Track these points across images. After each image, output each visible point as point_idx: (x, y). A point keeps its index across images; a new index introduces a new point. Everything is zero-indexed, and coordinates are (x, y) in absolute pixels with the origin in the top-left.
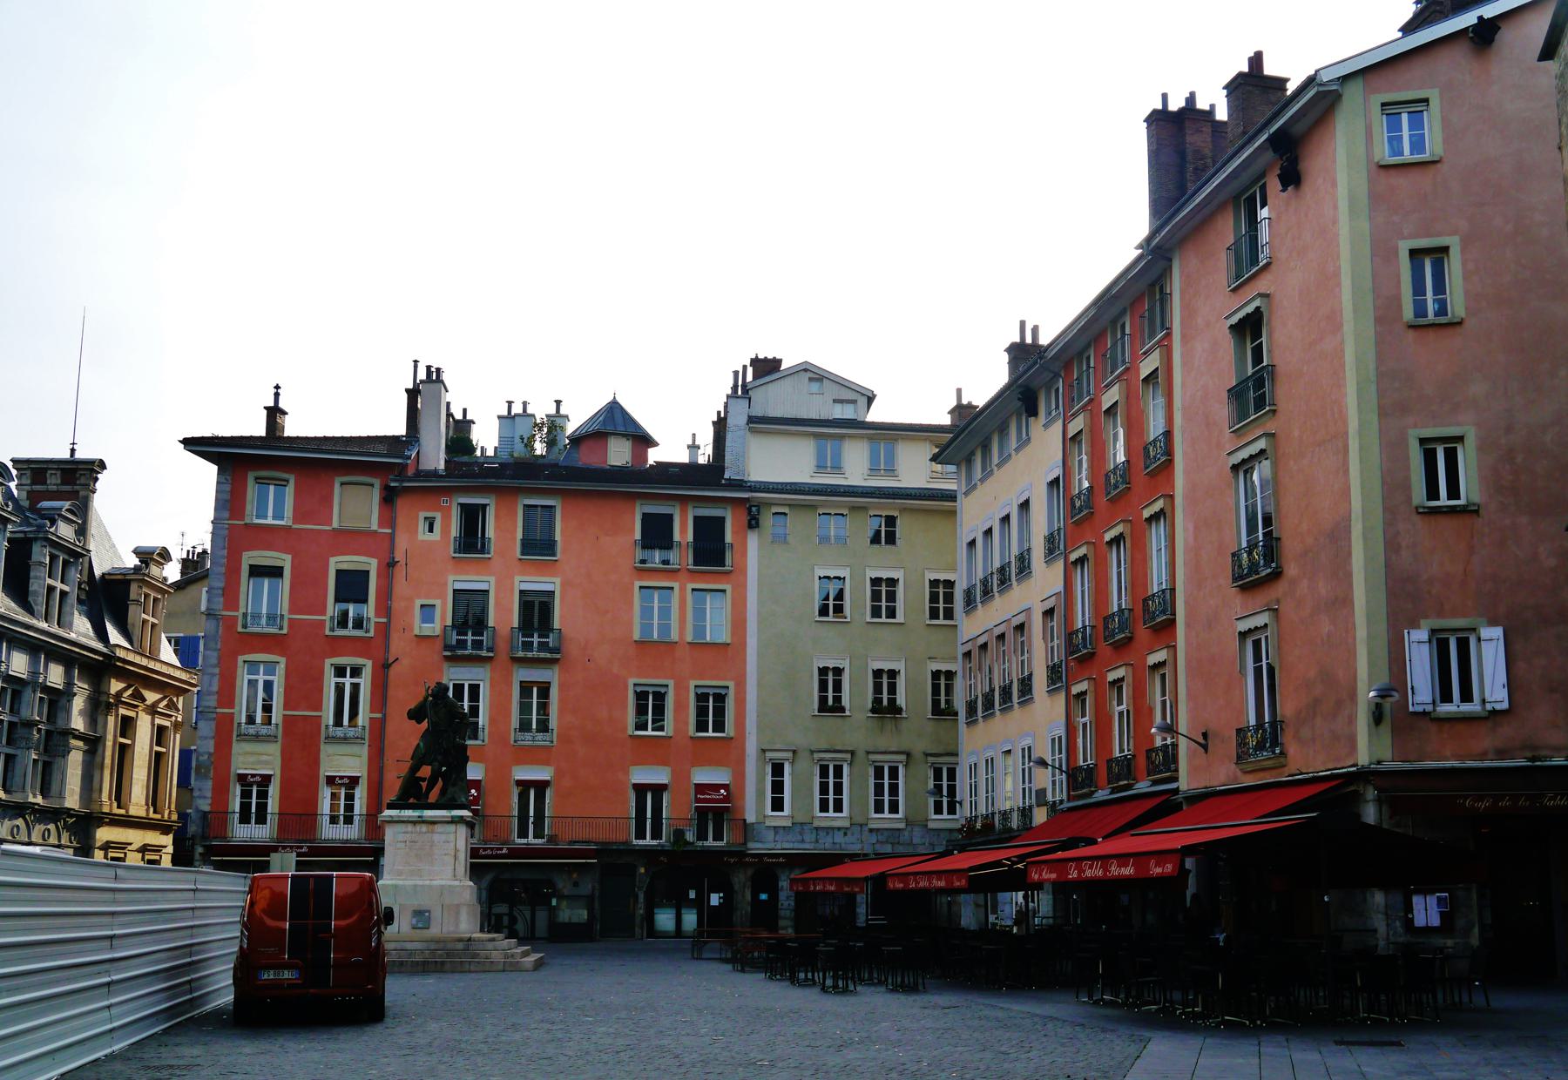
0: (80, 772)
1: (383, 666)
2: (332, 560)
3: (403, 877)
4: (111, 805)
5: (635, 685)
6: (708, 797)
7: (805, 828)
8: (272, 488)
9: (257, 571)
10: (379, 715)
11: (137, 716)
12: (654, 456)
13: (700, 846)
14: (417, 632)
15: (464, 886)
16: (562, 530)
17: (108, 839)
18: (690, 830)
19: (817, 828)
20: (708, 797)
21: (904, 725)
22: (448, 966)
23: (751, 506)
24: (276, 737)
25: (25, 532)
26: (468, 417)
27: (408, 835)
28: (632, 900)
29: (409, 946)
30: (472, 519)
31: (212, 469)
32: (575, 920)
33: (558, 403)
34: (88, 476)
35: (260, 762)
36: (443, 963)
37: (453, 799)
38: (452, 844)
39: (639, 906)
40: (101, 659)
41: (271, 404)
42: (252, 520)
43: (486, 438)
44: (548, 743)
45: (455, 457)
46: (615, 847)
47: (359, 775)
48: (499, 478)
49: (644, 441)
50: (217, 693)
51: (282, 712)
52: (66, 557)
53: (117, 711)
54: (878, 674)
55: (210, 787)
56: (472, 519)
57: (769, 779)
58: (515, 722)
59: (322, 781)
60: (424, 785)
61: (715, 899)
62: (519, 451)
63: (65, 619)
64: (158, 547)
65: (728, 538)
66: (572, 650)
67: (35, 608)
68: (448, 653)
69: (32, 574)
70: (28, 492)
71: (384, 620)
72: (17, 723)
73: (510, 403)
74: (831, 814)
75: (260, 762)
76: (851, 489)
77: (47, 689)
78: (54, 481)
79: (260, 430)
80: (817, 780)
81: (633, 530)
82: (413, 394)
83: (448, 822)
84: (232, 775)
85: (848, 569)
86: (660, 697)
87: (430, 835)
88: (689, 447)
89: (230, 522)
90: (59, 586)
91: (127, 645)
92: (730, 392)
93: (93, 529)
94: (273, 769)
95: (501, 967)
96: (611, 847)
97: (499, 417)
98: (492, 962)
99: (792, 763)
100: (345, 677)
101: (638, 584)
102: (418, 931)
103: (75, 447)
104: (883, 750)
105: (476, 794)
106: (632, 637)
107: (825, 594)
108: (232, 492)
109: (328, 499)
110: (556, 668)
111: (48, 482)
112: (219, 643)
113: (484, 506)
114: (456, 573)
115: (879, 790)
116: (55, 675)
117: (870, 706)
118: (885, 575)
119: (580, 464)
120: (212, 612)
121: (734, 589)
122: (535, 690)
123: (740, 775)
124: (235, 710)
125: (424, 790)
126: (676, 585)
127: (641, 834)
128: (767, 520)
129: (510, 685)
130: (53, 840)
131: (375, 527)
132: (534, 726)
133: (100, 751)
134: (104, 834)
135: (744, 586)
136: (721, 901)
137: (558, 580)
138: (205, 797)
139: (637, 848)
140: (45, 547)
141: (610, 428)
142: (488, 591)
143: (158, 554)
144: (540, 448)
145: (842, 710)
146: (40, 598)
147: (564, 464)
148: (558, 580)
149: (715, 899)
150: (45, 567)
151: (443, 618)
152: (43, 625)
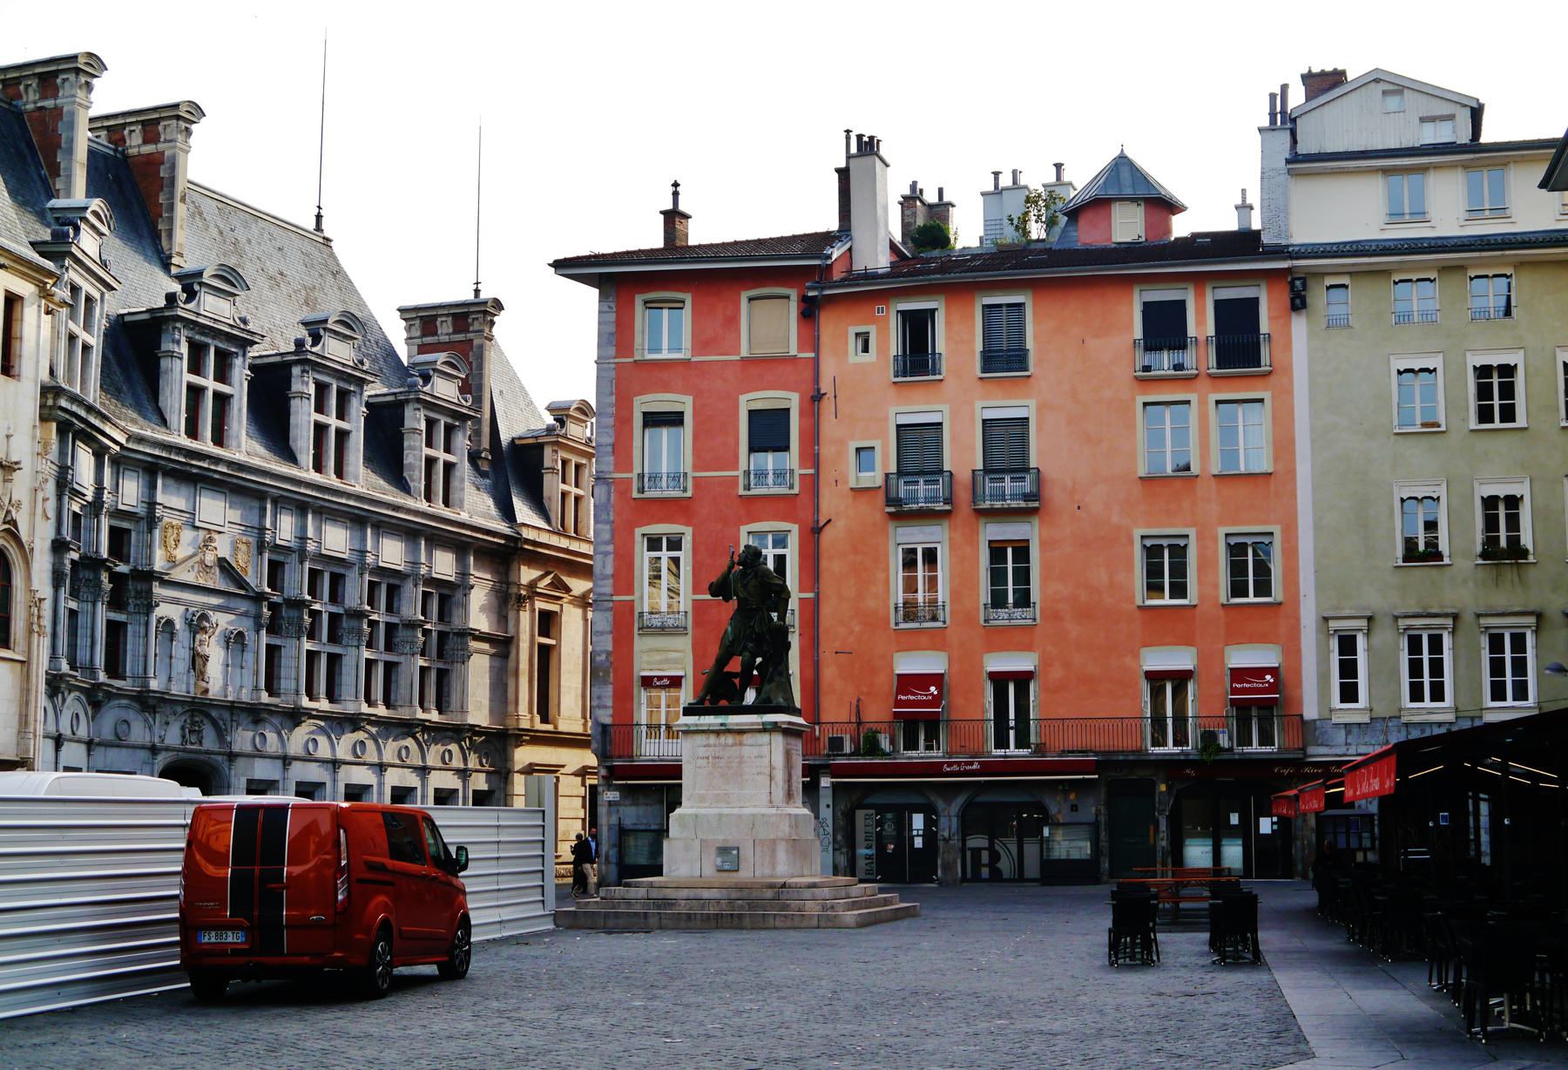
0: (487, 681)
1: (812, 529)
2: (743, 399)
3: (708, 804)
4: (532, 720)
5: (1143, 537)
6: (1247, 685)
7: (1390, 724)
9: (653, 420)
10: (811, 595)
11: (562, 610)
12: (1181, 227)
13: (1239, 754)
14: (853, 484)
15: (781, 815)
16: (1035, 337)
17: (532, 761)
18: (1223, 732)
19: (1406, 725)
20: (1247, 685)
21: (1532, 573)
22: (747, 922)
23: (1294, 279)
24: (685, 628)
25: (395, 394)
26: (946, 199)
27: (711, 749)
28: (1152, 827)
29: (706, 894)
30: (917, 329)
31: (592, 293)
32: (1075, 855)
33: (1058, 166)
34: (481, 320)
35: (667, 661)
36: (740, 916)
37: (769, 700)
38: (767, 760)
39: (1161, 835)
40: (503, 542)
41: (670, 207)
42: (643, 355)
43: (967, 232)
44: (1029, 622)
45: (922, 252)
46: (1121, 758)
47: (680, 673)
48: (945, 273)
49: (1164, 206)
50: (613, 576)
52: (449, 420)
53: (532, 605)
54: (1490, 503)
55: (611, 694)
56: (917, 329)
57: (1335, 658)
58: (984, 596)
59: (637, 683)
60: (737, 681)
61: (1266, 825)
62: (1009, 235)
63: (454, 496)
64: (574, 401)
65: (1264, 327)
66: (1056, 495)
67: (412, 485)
68: (892, 509)
69: (406, 444)
70: (419, 346)
71: (811, 471)
72: (398, 624)
73: (996, 174)
74: (1427, 703)
75: (667, 661)
76: (1439, 243)
77: (431, 581)
78: (445, 331)
79: (656, 241)
80: (1404, 658)
81: (1130, 327)
82: (844, 174)
83: (759, 731)
84: (635, 678)
85: (1440, 356)
86: (1179, 552)
87: (738, 748)
89: (617, 360)
91: (542, 524)
92: (1266, 123)
93: (493, 380)
94: (684, 668)
95: (815, 922)
96: (1115, 758)
98: (803, 915)
99: (1368, 634)
100: (661, 550)
101: (1141, 399)
102: (725, 874)
103: (480, 287)
104: (1500, 610)
105: (936, 693)
106: (1136, 472)
108: (618, 323)
109: (732, 321)
110: (1036, 521)
111: (439, 332)
112: (612, 513)
113: (933, 311)
114: (1144, 393)
115: (1497, 668)
116: (444, 565)
117: (1479, 549)
118: (1495, 360)
119: (1079, 246)
120: (601, 475)
121: (1274, 398)
122: (1010, 551)
123: (1292, 650)
124: (635, 597)
126: (1193, 397)
127: (1159, 740)
128: (1318, 296)
129: (974, 544)
130: (457, 763)
131: (793, 351)
132: (1011, 600)
133: (513, 655)
134: (524, 755)
135: (1289, 392)
136: (1275, 827)
137: (1032, 403)
138: (606, 707)
139: (1152, 758)
140: (419, 409)
141: (1112, 192)
142: (940, 424)
143: (578, 409)
144: (1036, 231)
145: (1439, 556)
146: (417, 472)
147: (1058, 248)
148: (1032, 403)
149: (1266, 825)
150: (420, 434)
151: (885, 463)
152: (423, 505)
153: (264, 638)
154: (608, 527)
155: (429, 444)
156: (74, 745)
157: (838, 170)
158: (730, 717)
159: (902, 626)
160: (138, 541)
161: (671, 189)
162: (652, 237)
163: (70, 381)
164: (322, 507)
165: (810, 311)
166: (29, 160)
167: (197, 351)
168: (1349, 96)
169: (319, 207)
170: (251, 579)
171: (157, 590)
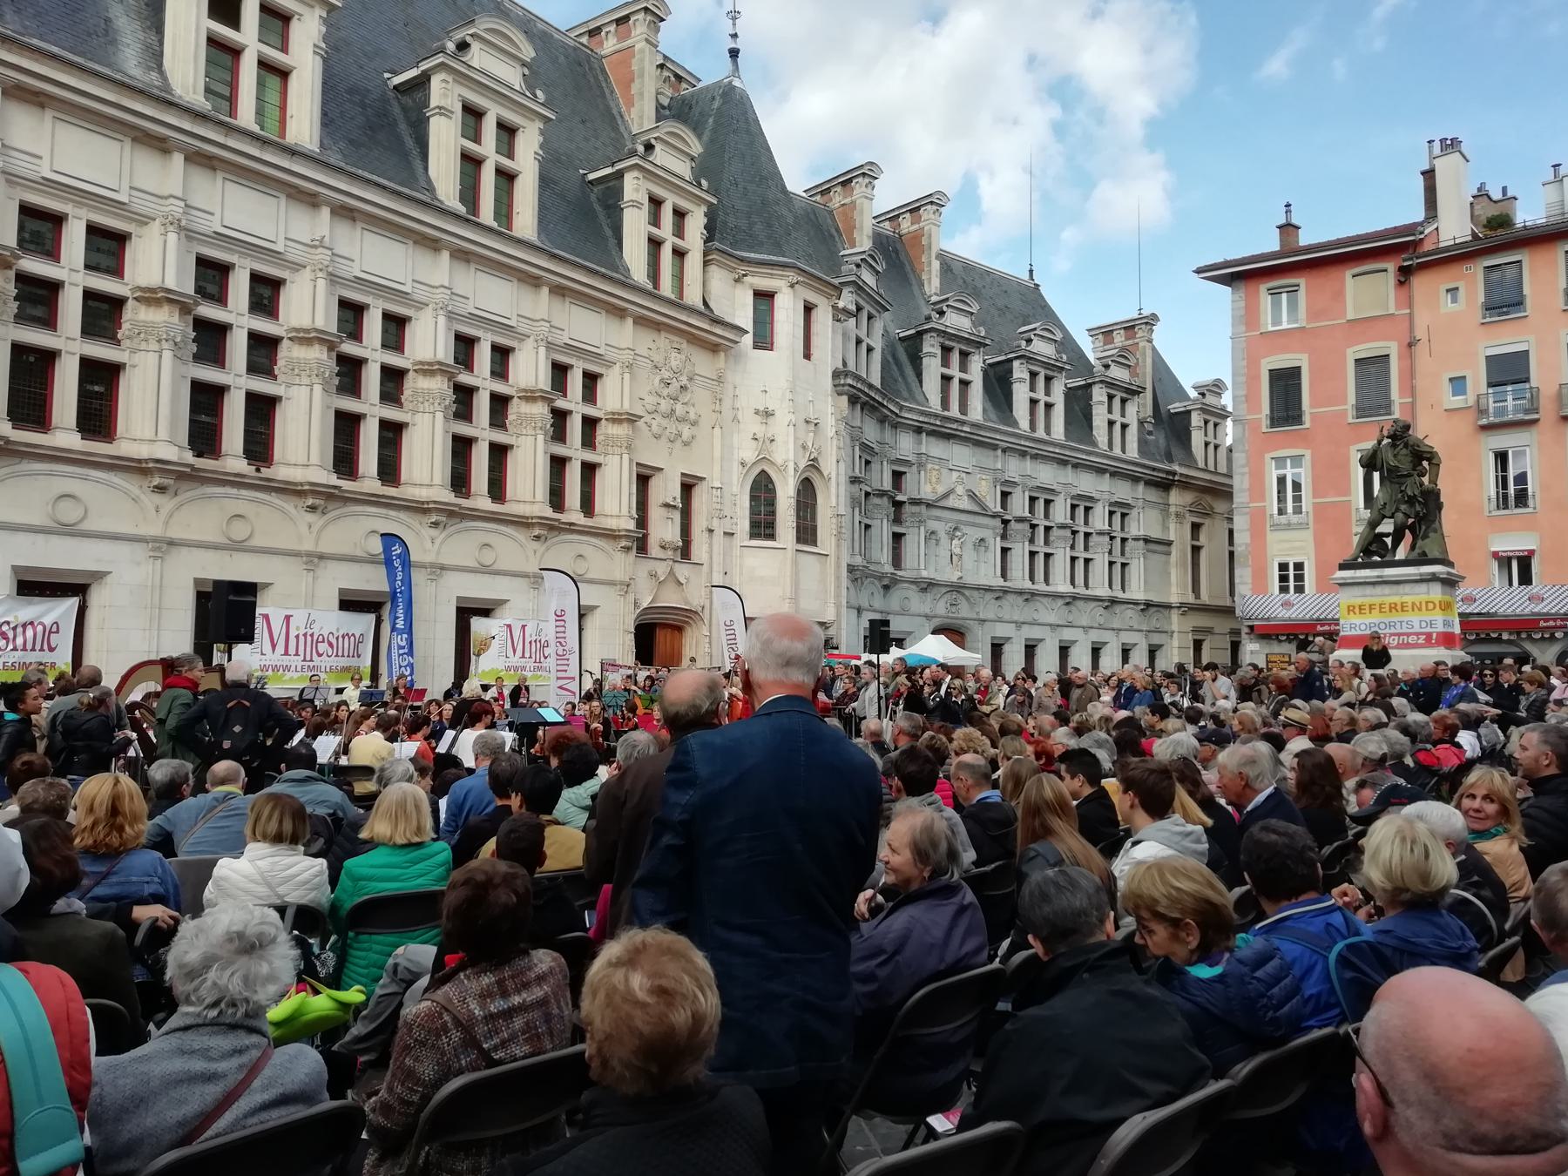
8: (1284, 296)
10: (1289, 461)
26: (1509, 194)
37: (1424, 554)
41: (1283, 221)
51: (1311, 500)
52: (1124, 395)
60: (1389, 541)
82: (1429, 175)
108: (1247, 308)
109: (1340, 295)
131: (1392, 310)
154: (1244, 455)
159: (1494, 513)
161: (1285, 209)
162: (1272, 243)
164: (1037, 454)
165: (1405, 274)
166: (837, 239)
167: (946, 350)
170: (990, 505)
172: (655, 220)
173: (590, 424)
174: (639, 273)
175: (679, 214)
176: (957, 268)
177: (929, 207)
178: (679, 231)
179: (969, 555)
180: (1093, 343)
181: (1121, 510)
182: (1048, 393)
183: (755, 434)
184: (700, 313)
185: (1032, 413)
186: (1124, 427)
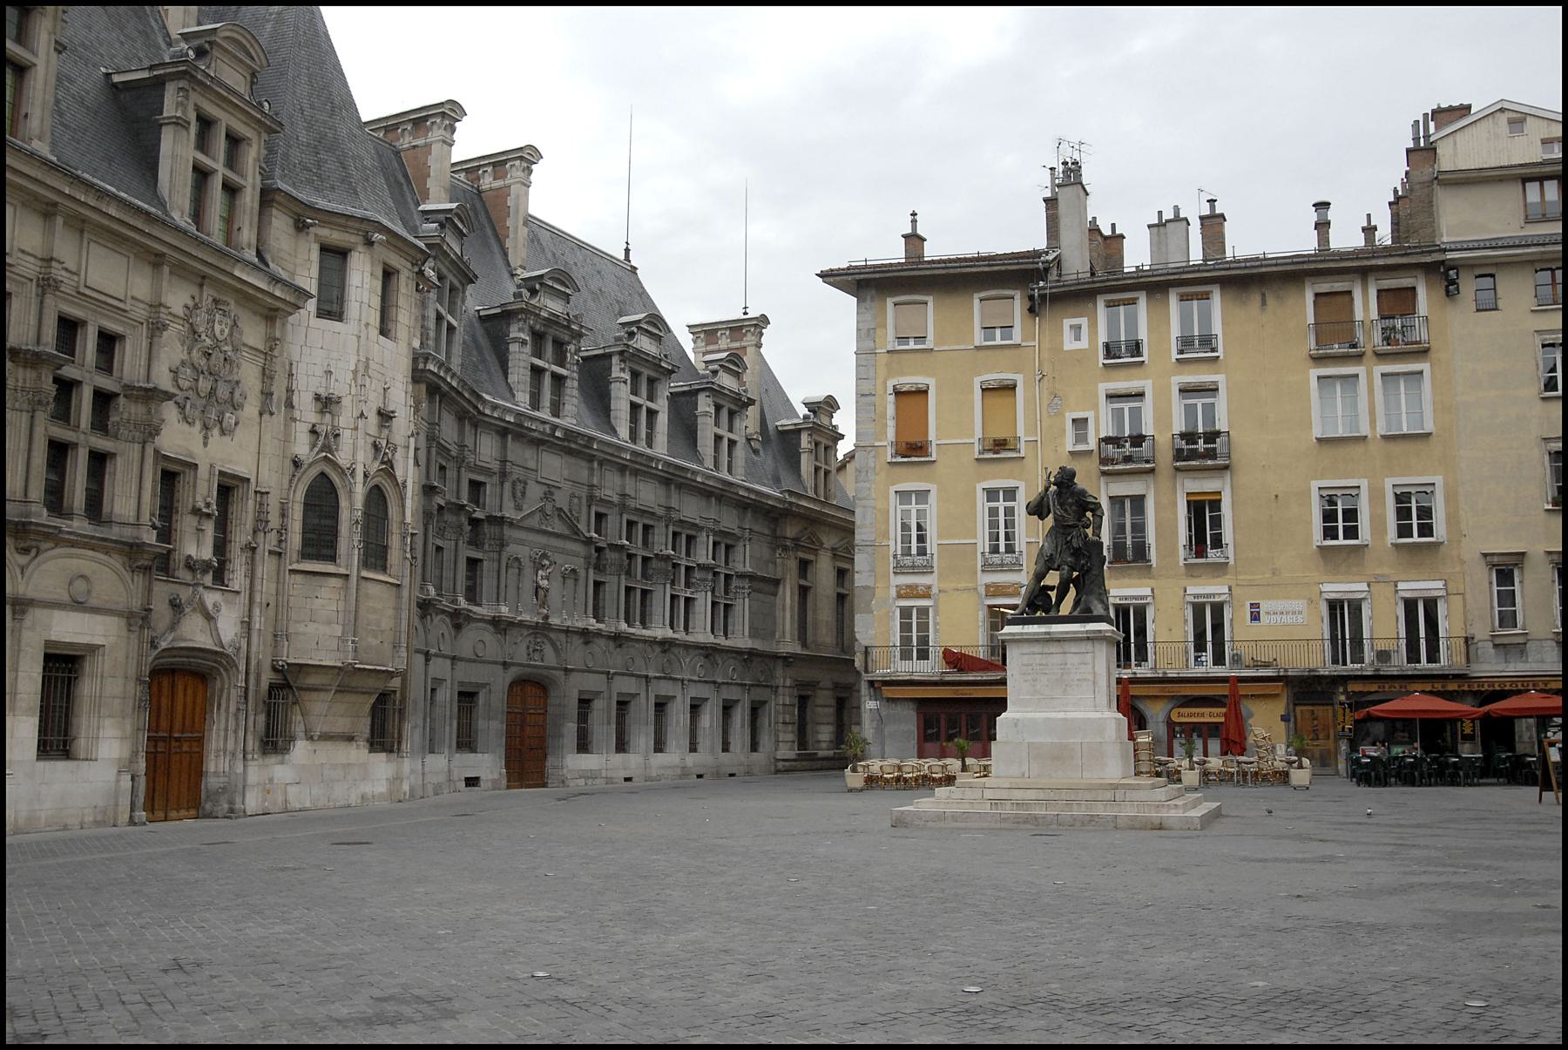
33: (1212, 202)
37: (1089, 610)
41: (909, 231)
43: (1137, 255)
60: (1053, 594)
82: (1051, 203)
88: (1364, 229)
90: (727, 435)
97: (1149, 226)
107: (1552, 366)
125: (1054, 600)
153: (592, 576)
155: (717, 424)
156: (440, 660)
157: (1045, 200)
158: (1054, 625)
160: (491, 492)
161: (910, 218)
163: (437, 350)
167: (538, 337)
168: (1478, 124)
169: (627, 243)
170: (582, 527)
171: (507, 532)
172: (203, 144)
173: (103, 400)
174: (180, 215)
175: (234, 141)
176: (545, 236)
177: (517, 163)
178: (232, 161)
179: (556, 590)
180: (695, 342)
181: (726, 543)
182: (651, 398)
183: (314, 426)
184: (255, 267)
185: (634, 419)
186: (732, 443)
